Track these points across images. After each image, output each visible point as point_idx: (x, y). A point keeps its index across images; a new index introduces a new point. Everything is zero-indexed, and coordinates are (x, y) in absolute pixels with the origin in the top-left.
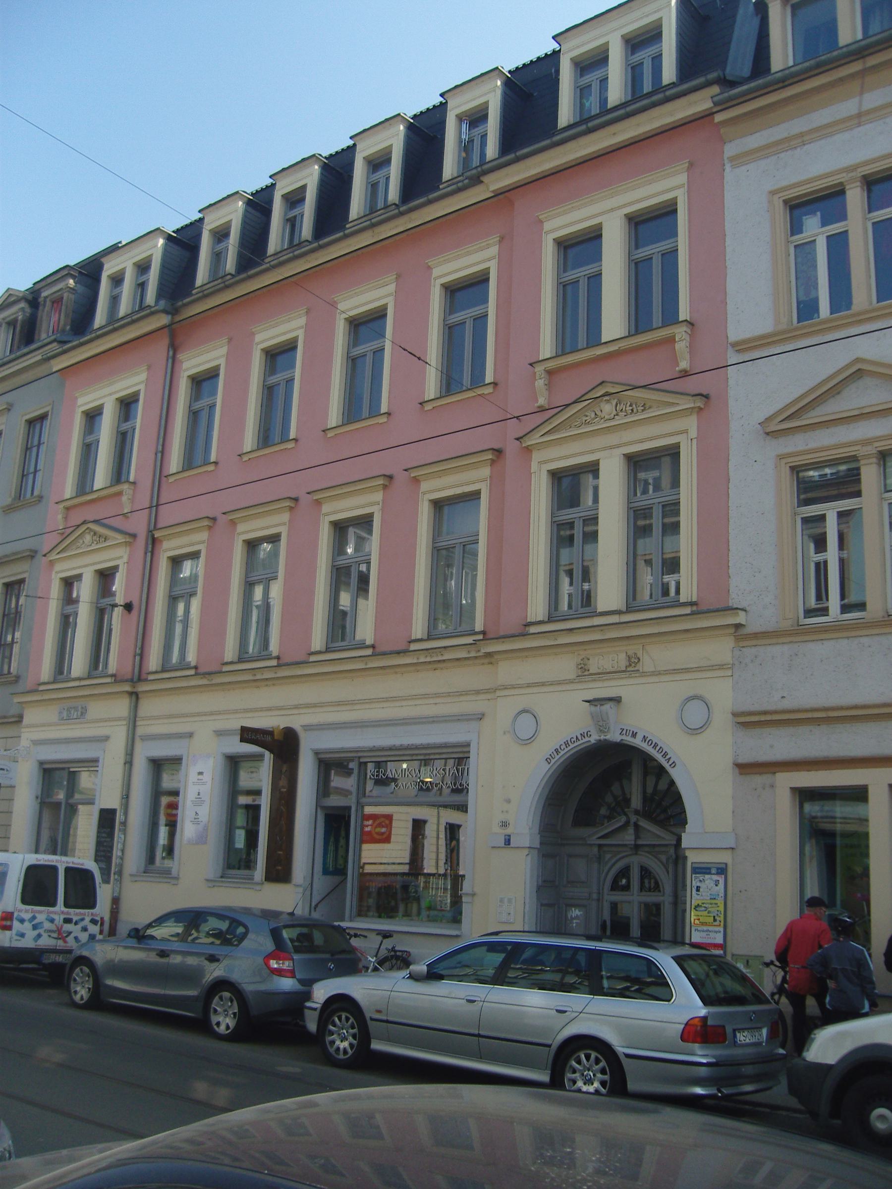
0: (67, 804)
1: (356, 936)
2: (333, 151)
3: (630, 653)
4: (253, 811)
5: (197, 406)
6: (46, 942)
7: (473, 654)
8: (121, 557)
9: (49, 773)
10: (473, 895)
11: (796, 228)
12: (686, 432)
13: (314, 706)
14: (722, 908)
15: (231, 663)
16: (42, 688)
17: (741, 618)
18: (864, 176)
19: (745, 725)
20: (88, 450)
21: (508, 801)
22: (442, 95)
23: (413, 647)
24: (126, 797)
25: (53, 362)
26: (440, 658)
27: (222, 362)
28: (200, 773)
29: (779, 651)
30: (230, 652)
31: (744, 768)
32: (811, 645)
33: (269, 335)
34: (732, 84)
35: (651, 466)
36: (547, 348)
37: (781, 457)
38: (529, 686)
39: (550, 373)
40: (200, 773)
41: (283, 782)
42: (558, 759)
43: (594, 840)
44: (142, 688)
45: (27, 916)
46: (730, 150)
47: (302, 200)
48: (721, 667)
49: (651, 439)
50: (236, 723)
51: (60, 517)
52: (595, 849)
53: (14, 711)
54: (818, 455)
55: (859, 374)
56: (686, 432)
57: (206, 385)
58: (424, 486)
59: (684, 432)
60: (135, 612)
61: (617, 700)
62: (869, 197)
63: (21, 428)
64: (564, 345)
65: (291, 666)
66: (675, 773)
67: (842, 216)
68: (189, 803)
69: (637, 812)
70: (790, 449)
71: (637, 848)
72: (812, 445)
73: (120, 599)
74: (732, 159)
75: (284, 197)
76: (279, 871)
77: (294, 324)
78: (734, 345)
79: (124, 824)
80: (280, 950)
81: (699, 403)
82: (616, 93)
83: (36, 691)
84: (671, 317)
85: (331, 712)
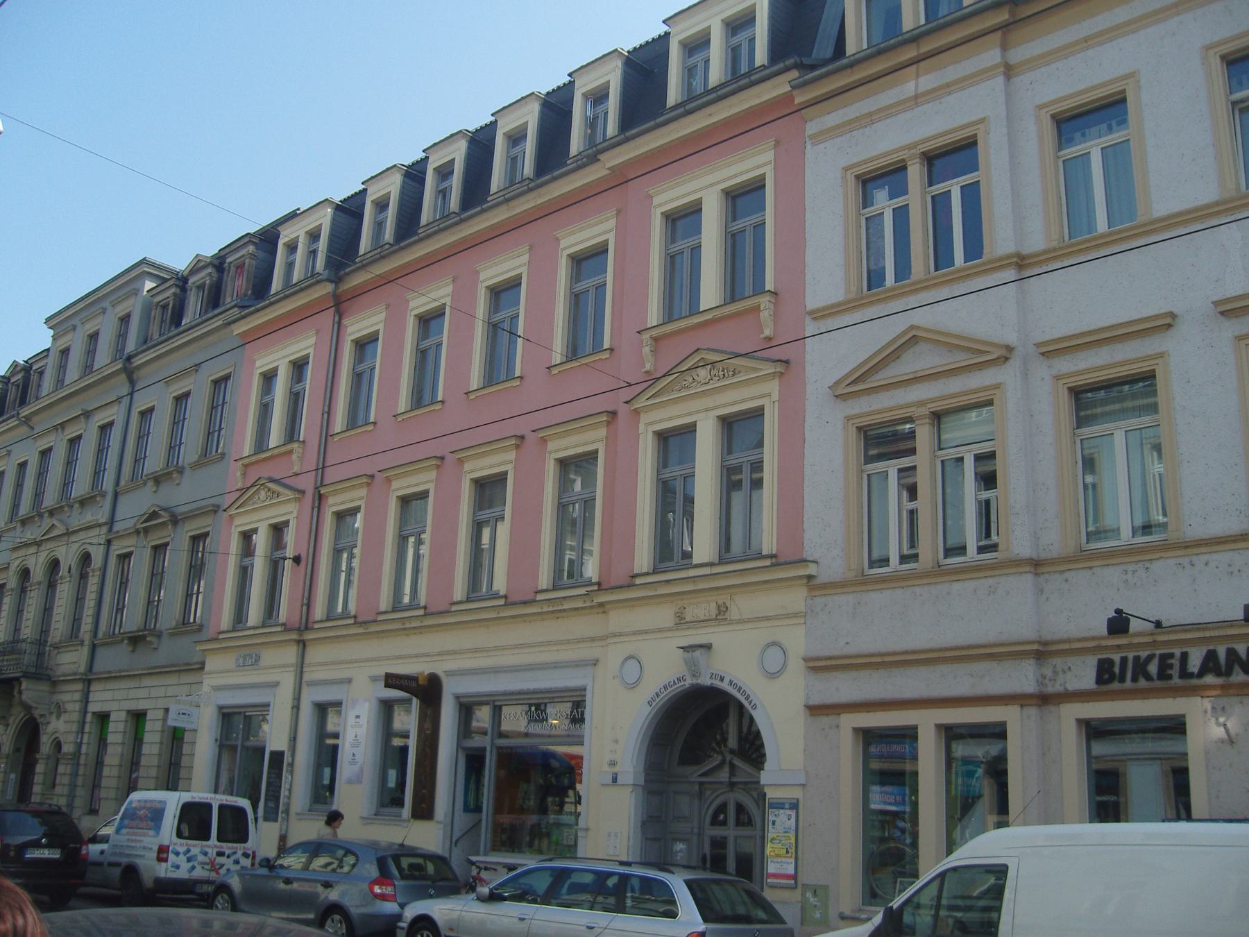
0: (243, 746)
1: (486, 869)
2: (550, 89)
3: (720, 602)
4: (404, 750)
5: (360, 368)
6: (199, 873)
7: (588, 604)
8: (291, 512)
9: (227, 716)
10: (587, 830)
11: (866, 201)
12: (769, 395)
13: (455, 652)
14: (793, 840)
15: (385, 612)
16: (221, 636)
17: (812, 570)
18: (923, 153)
19: (815, 669)
20: (265, 409)
21: (616, 742)
22: (570, 75)
23: (539, 597)
24: (293, 739)
25: (233, 327)
26: (560, 608)
27: (524, 271)
28: (358, 717)
29: (845, 600)
30: (384, 602)
31: (815, 710)
32: (873, 595)
33: (420, 303)
34: (813, 67)
35: (739, 428)
36: (654, 317)
37: (849, 419)
38: (634, 633)
39: (656, 340)
40: (358, 717)
41: (428, 725)
42: (659, 702)
43: (694, 778)
44: (309, 636)
45: (182, 849)
46: (811, 128)
47: (607, 96)
48: (796, 615)
49: (740, 402)
50: (381, 670)
51: (239, 474)
52: (697, 787)
53: (197, 658)
54: (1134, 366)
55: (914, 340)
56: (769, 395)
57: (433, 324)
58: (551, 446)
59: (764, 393)
60: (303, 564)
61: (708, 647)
62: (930, 171)
63: (170, 403)
64: (669, 314)
65: (433, 616)
66: (755, 714)
67: (905, 192)
68: (347, 745)
69: (732, 752)
70: (856, 411)
71: (732, 785)
72: (875, 407)
73: (290, 552)
74: (812, 137)
75: (586, 96)
76: (424, 810)
77: (517, 262)
78: (811, 313)
79: (291, 765)
80: (384, 877)
81: (780, 368)
82: (716, 74)
83: (217, 639)
84: (759, 290)
85: (474, 660)
